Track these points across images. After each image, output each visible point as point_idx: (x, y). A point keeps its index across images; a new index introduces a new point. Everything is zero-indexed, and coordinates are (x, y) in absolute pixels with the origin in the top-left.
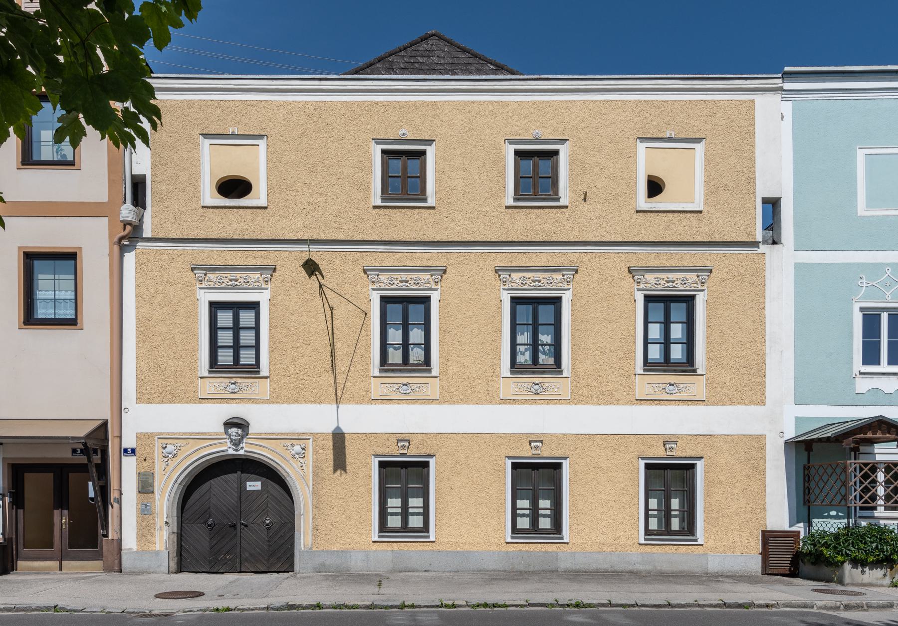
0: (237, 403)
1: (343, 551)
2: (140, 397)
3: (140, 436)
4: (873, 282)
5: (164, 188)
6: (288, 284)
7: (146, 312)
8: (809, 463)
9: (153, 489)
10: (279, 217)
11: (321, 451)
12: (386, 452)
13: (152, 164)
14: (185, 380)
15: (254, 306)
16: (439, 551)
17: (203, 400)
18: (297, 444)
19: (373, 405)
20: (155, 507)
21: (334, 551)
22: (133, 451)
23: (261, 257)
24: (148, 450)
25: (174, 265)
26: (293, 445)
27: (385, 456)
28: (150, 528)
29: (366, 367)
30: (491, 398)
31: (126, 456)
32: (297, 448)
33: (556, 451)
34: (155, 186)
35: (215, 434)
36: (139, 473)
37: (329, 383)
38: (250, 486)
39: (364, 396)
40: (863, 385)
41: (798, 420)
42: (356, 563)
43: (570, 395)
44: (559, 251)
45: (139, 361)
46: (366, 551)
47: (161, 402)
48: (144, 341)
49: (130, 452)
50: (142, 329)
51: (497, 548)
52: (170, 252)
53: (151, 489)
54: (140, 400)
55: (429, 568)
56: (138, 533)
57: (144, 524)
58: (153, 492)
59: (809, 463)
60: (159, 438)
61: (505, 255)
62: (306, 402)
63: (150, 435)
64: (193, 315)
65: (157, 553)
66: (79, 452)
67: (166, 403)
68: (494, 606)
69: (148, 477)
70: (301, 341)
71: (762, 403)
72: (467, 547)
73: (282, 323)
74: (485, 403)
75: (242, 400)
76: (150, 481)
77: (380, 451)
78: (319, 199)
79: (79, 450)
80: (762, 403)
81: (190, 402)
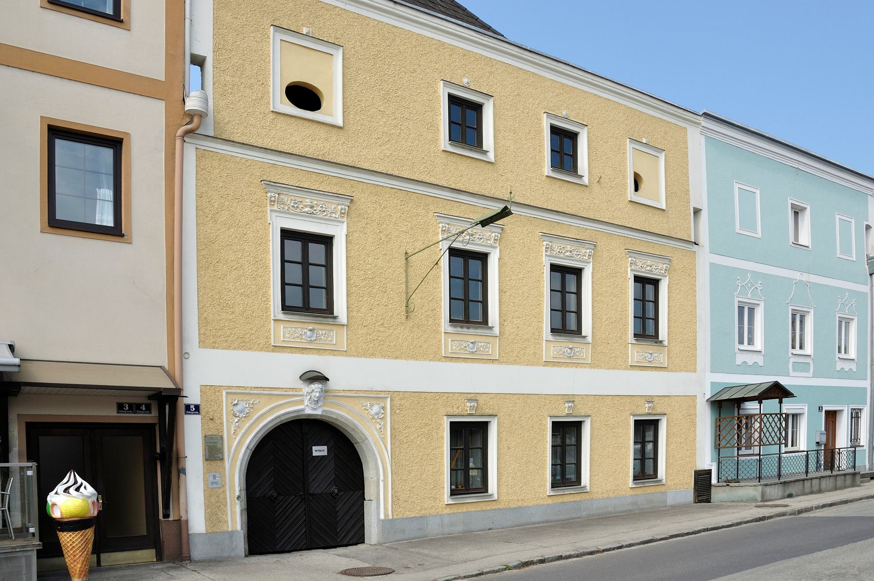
0: (313, 354)
1: (420, 517)
2: (203, 339)
3: (204, 389)
4: (748, 277)
5: (228, 78)
6: (364, 221)
7: (209, 231)
8: (720, 417)
9: (223, 455)
10: (354, 142)
11: (398, 411)
12: (456, 413)
13: (215, 45)
14: (256, 322)
15: (327, 241)
16: (500, 509)
17: (277, 348)
18: (376, 404)
19: (444, 363)
20: (225, 478)
21: (413, 517)
22: (197, 408)
23: (336, 184)
24: (215, 408)
25: (241, 177)
26: (372, 405)
27: (638, 271)
28: (220, 504)
29: (437, 322)
30: (535, 360)
31: (189, 414)
32: (376, 409)
33: (581, 411)
34: (218, 74)
35: (291, 390)
36: (205, 436)
37: (404, 337)
38: (324, 451)
39: (436, 353)
40: (740, 359)
41: (713, 384)
42: (433, 528)
43: (590, 360)
44: (583, 226)
45: (201, 293)
46: (441, 515)
47: (228, 348)
48: (207, 268)
49: (194, 409)
50: (204, 252)
51: (541, 502)
52: (238, 159)
53: (220, 455)
54: (203, 344)
55: (493, 527)
56: (207, 511)
57: (213, 500)
58: (222, 459)
59: (720, 417)
60: (545, 235)
61: (546, 222)
62: (383, 356)
63: (216, 389)
64: (262, 242)
65: (232, 534)
66: (127, 408)
67: (235, 349)
68: (542, 561)
69: (215, 441)
70: (377, 287)
71: (695, 371)
72: (520, 504)
73: (358, 265)
74: (533, 365)
75: (319, 351)
76: (219, 446)
77: (451, 411)
78: (393, 131)
79: (127, 405)
80: (695, 371)
81: (262, 350)
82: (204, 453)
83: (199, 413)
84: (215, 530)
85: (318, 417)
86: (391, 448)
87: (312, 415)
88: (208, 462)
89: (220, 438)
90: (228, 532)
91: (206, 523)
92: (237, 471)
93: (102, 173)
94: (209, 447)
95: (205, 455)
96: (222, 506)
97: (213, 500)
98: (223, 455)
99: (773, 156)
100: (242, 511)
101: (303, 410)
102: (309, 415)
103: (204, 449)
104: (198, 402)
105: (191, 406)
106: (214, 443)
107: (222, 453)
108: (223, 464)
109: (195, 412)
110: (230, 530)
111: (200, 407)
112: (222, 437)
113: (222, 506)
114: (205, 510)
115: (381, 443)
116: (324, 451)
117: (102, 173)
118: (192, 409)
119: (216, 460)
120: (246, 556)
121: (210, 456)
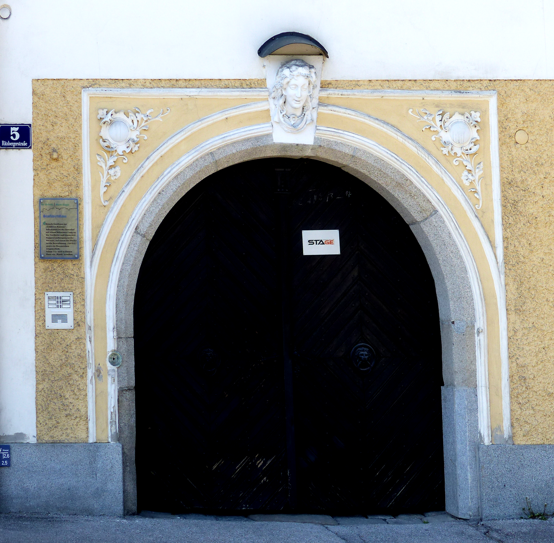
58: (76, 257)
82: (37, 241)
83: (28, 146)
84: (58, 435)
85: (308, 153)
86: (505, 239)
87: (291, 146)
88: (47, 264)
89: (72, 205)
90: (86, 444)
91: (37, 417)
92: (149, 198)
93: (124, 338)
94: (49, 226)
95: (38, 246)
96: (75, 377)
97: (54, 358)
98: (79, 249)
99: (352, 138)
100: (121, 391)
101: (269, 136)
102: (284, 147)
103: (38, 233)
104: (26, 118)
105: (12, 129)
106: (60, 216)
107: (77, 242)
108: (79, 269)
109: (19, 144)
110: (91, 440)
111: (32, 130)
112: (77, 203)
113: (75, 377)
114: (37, 384)
115: (476, 224)
116: (331, 242)
117: (124, 338)
118: (14, 136)
119: (64, 259)
120: (127, 513)
121: (49, 252)
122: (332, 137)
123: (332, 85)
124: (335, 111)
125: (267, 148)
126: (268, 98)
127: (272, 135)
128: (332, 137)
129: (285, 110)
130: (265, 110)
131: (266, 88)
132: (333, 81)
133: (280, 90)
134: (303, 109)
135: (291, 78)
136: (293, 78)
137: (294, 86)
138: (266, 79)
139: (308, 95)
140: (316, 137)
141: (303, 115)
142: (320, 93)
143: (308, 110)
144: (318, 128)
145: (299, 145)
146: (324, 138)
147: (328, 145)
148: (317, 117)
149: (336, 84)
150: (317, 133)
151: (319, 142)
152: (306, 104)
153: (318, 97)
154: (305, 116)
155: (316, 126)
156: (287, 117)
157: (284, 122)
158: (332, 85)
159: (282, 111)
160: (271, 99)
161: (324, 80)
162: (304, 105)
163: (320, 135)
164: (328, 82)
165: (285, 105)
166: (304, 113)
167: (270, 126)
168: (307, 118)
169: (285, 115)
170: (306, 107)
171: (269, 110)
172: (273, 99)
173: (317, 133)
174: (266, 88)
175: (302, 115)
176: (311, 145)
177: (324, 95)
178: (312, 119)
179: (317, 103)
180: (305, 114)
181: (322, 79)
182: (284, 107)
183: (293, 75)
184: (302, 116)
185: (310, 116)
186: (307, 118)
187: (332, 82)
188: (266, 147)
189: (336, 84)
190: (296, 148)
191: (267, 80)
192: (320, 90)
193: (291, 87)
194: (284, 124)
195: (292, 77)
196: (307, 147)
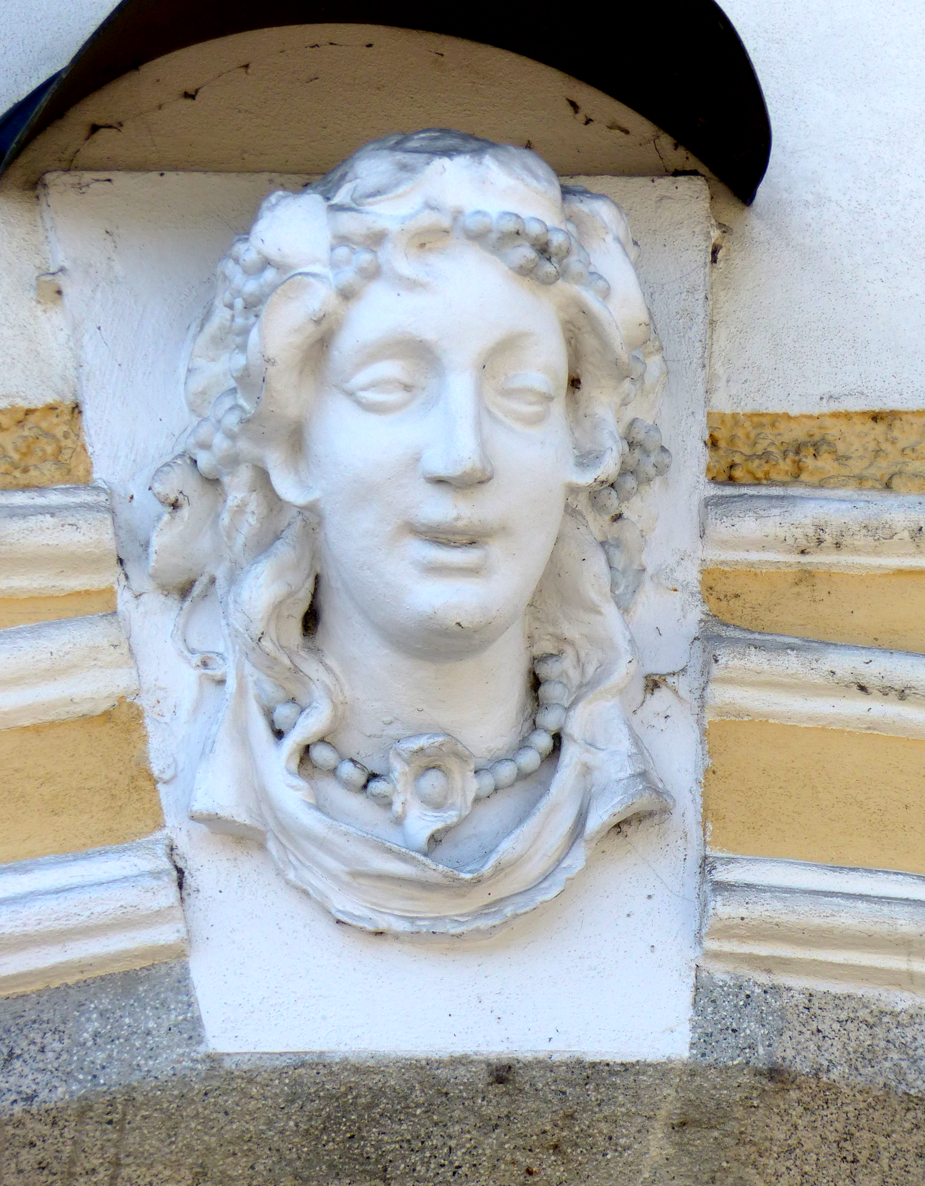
122: (896, 962)
123: (841, 459)
124: (902, 695)
125: (132, 1139)
126: (110, 592)
127: (182, 984)
128: (896, 962)
129: (318, 692)
130: (86, 719)
131: (86, 483)
132: (842, 425)
133: (245, 474)
134: (536, 683)
135: (348, 275)
136: (372, 274)
137: (390, 369)
138: (76, 409)
139: (573, 490)
140: (720, 973)
141: (543, 741)
142: (720, 529)
143: (585, 688)
144: (722, 874)
145: (522, 1079)
146: (819, 985)
147: (868, 1056)
148: (711, 772)
149: (878, 452)
150: (726, 931)
151: (750, 1027)
152: (570, 631)
153: (691, 575)
154: (570, 754)
155: (706, 865)
156: (347, 770)
157: (310, 820)
158: (841, 459)
159: (283, 713)
160: (154, 601)
161: (748, 407)
162: (546, 646)
163: (763, 950)
164: (798, 433)
165: (315, 651)
166: (550, 719)
167: (156, 875)
168: (587, 770)
169: (321, 754)
170: (567, 663)
171: (137, 716)
172: (173, 602)
173: (726, 931)
174: (86, 483)
175: (523, 744)
176: (662, 1070)
177: (755, 556)
178: (643, 775)
179: (694, 631)
180: (557, 739)
181: (723, 404)
182: (311, 667)
183: (377, 239)
184: (530, 759)
185: (625, 745)
186: (587, 770)
187: (834, 430)
188: (119, 1125)
189: (878, 452)
190: (490, 1126)
191: (89, 412)
192: (708, 503)
193: (362, 378)
194: (322, 844)
195: (365, 258)
196: (622, 1102)
